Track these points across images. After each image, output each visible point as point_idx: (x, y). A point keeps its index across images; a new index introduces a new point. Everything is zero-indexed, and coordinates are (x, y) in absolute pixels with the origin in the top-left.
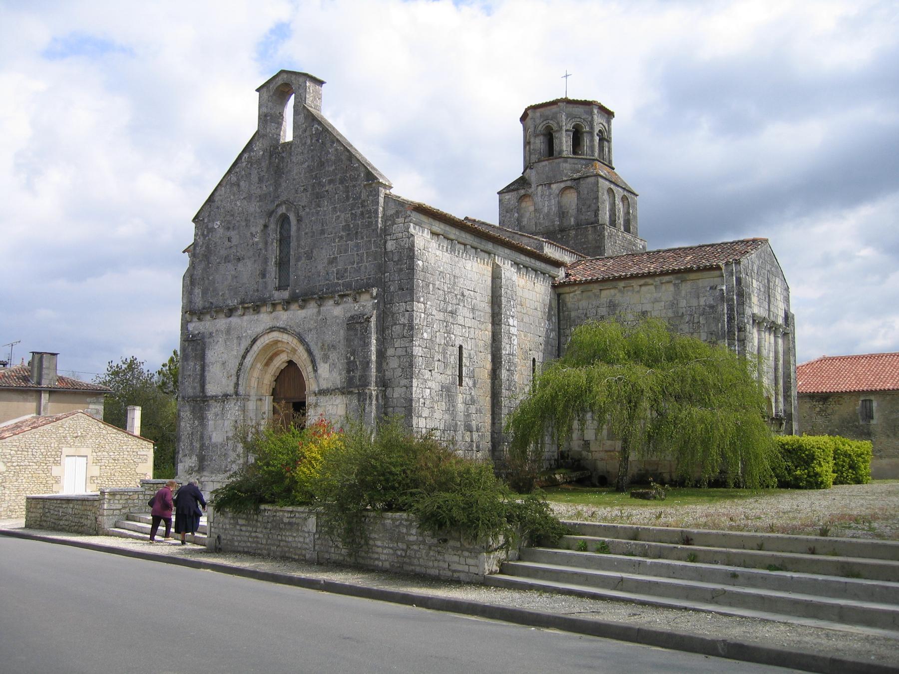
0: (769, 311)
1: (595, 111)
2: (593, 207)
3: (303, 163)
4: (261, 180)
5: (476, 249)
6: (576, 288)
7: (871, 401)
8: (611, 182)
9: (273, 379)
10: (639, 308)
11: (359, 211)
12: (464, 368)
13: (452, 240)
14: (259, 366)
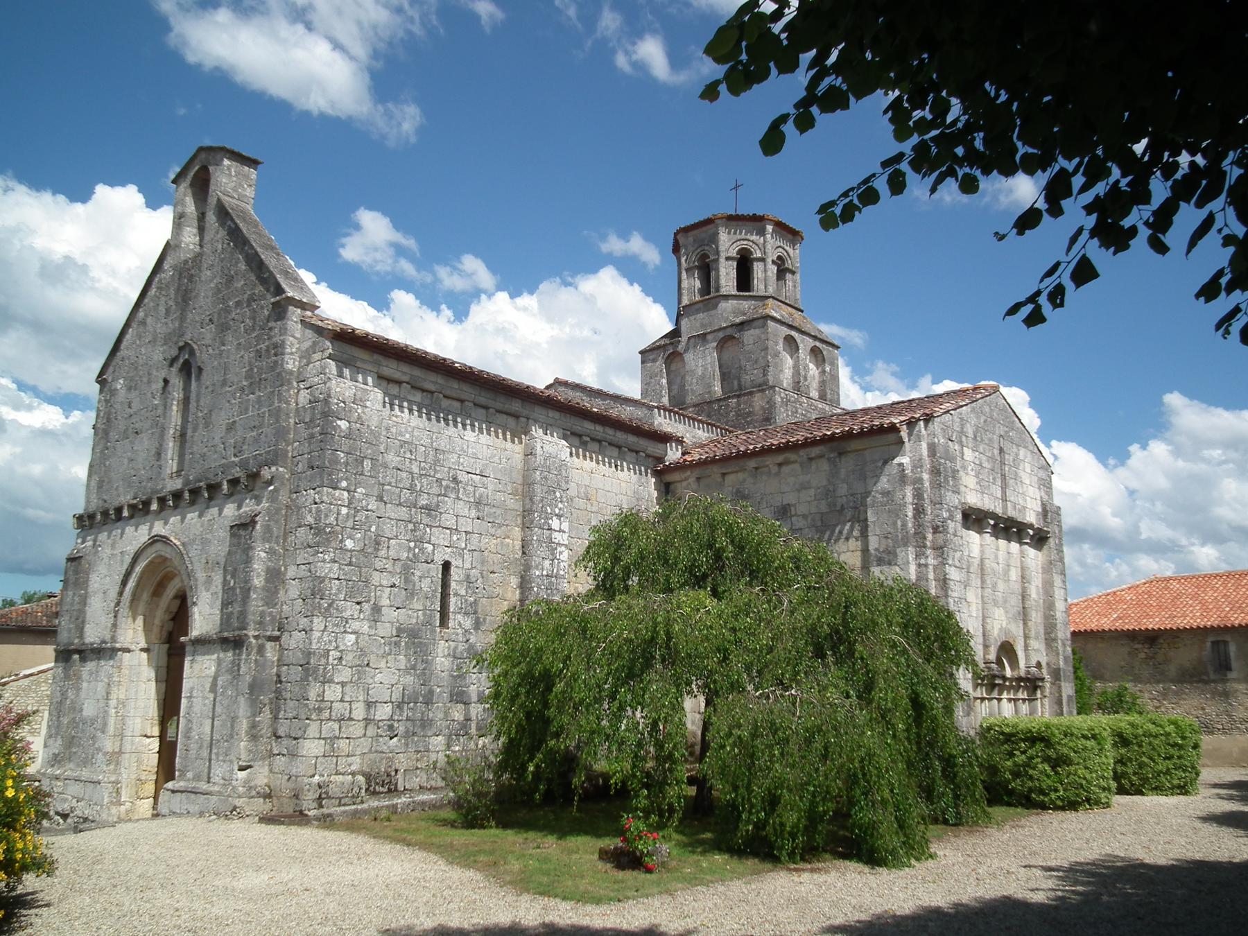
0: (1004, 500)
1: (770, 228)
2: (762, 362)
3: (211, 281)
5: (486, 408)
6: (689, 473)
7: (1226, 643)
8: (791, 327)
9: (167, 617)
10: (778, 501)
12: (453, 600)
13: (432, 393)
14: (145, 596)
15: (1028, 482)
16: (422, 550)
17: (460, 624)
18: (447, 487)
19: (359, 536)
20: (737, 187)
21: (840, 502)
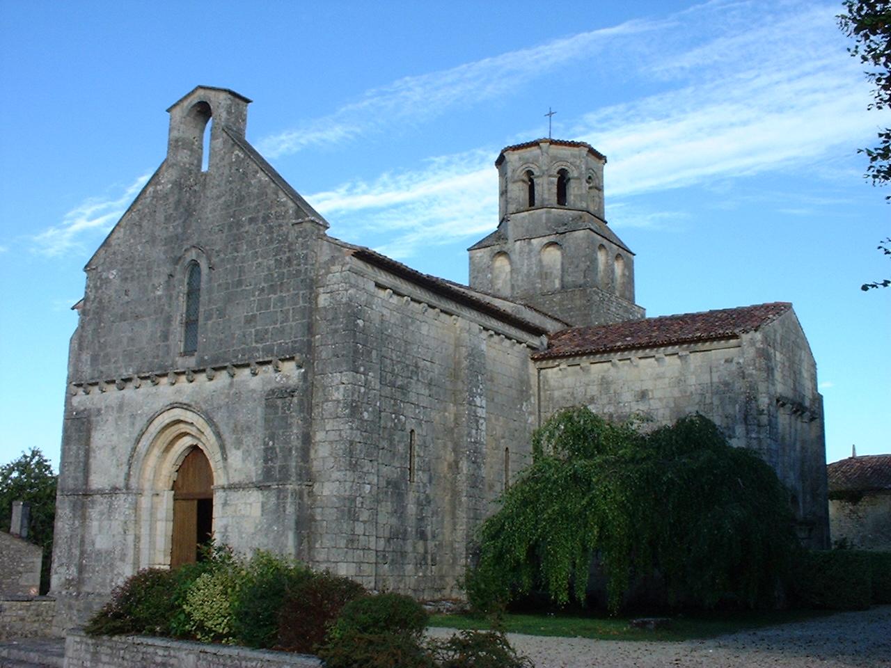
4: (168, 219)
10: (638, 387)
11: (285, 257)
17: (421, 479)
19: (370, 409)
20: (550, 114)
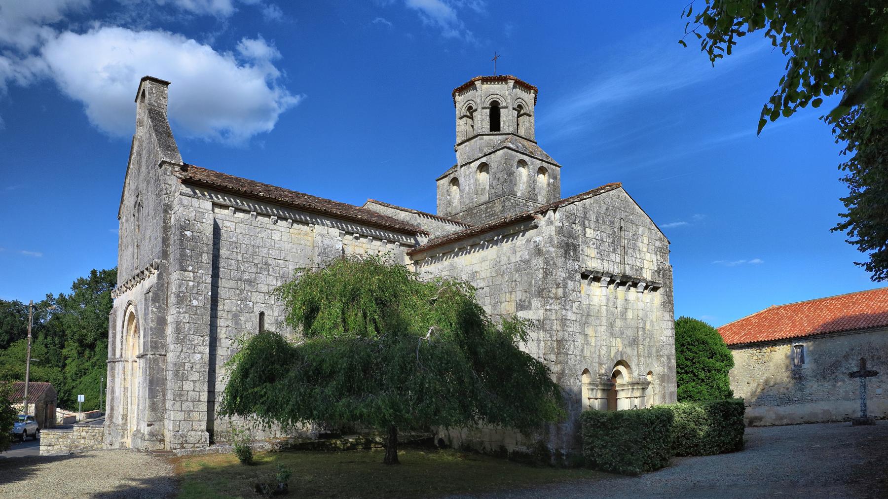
15: (645, 250)
16: (246, 305)
18: (261, 268)
21: (503, 268)
